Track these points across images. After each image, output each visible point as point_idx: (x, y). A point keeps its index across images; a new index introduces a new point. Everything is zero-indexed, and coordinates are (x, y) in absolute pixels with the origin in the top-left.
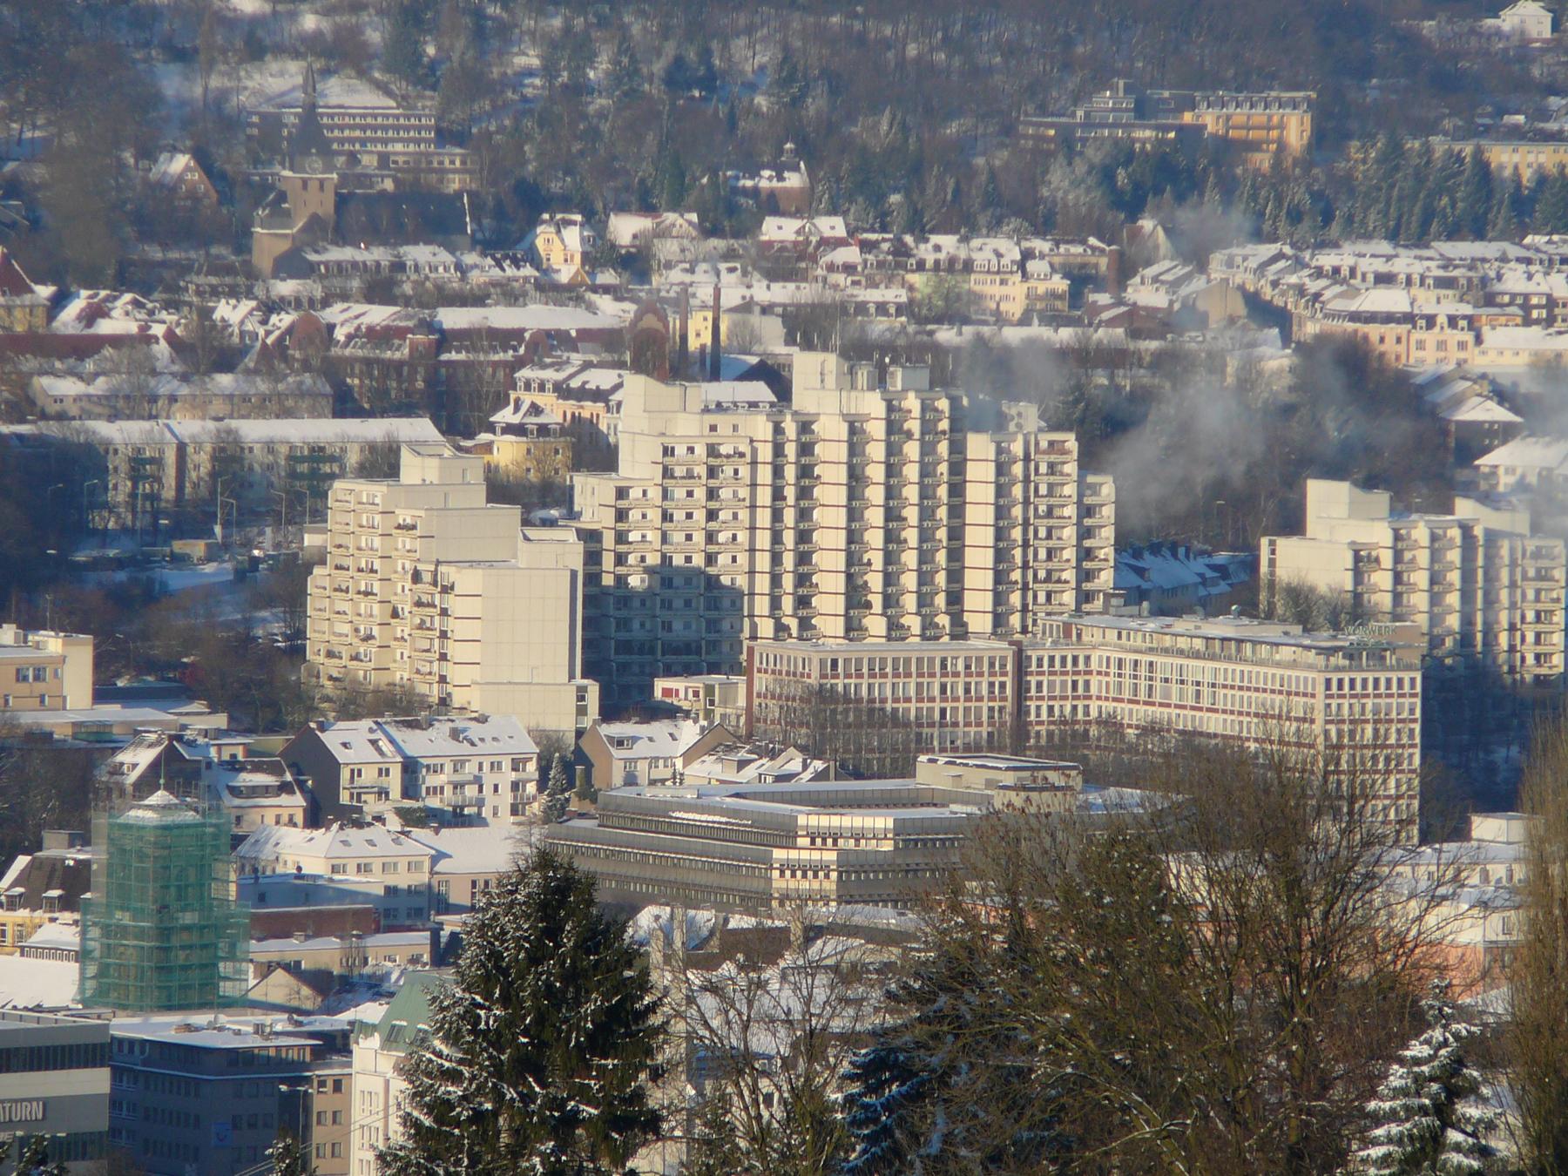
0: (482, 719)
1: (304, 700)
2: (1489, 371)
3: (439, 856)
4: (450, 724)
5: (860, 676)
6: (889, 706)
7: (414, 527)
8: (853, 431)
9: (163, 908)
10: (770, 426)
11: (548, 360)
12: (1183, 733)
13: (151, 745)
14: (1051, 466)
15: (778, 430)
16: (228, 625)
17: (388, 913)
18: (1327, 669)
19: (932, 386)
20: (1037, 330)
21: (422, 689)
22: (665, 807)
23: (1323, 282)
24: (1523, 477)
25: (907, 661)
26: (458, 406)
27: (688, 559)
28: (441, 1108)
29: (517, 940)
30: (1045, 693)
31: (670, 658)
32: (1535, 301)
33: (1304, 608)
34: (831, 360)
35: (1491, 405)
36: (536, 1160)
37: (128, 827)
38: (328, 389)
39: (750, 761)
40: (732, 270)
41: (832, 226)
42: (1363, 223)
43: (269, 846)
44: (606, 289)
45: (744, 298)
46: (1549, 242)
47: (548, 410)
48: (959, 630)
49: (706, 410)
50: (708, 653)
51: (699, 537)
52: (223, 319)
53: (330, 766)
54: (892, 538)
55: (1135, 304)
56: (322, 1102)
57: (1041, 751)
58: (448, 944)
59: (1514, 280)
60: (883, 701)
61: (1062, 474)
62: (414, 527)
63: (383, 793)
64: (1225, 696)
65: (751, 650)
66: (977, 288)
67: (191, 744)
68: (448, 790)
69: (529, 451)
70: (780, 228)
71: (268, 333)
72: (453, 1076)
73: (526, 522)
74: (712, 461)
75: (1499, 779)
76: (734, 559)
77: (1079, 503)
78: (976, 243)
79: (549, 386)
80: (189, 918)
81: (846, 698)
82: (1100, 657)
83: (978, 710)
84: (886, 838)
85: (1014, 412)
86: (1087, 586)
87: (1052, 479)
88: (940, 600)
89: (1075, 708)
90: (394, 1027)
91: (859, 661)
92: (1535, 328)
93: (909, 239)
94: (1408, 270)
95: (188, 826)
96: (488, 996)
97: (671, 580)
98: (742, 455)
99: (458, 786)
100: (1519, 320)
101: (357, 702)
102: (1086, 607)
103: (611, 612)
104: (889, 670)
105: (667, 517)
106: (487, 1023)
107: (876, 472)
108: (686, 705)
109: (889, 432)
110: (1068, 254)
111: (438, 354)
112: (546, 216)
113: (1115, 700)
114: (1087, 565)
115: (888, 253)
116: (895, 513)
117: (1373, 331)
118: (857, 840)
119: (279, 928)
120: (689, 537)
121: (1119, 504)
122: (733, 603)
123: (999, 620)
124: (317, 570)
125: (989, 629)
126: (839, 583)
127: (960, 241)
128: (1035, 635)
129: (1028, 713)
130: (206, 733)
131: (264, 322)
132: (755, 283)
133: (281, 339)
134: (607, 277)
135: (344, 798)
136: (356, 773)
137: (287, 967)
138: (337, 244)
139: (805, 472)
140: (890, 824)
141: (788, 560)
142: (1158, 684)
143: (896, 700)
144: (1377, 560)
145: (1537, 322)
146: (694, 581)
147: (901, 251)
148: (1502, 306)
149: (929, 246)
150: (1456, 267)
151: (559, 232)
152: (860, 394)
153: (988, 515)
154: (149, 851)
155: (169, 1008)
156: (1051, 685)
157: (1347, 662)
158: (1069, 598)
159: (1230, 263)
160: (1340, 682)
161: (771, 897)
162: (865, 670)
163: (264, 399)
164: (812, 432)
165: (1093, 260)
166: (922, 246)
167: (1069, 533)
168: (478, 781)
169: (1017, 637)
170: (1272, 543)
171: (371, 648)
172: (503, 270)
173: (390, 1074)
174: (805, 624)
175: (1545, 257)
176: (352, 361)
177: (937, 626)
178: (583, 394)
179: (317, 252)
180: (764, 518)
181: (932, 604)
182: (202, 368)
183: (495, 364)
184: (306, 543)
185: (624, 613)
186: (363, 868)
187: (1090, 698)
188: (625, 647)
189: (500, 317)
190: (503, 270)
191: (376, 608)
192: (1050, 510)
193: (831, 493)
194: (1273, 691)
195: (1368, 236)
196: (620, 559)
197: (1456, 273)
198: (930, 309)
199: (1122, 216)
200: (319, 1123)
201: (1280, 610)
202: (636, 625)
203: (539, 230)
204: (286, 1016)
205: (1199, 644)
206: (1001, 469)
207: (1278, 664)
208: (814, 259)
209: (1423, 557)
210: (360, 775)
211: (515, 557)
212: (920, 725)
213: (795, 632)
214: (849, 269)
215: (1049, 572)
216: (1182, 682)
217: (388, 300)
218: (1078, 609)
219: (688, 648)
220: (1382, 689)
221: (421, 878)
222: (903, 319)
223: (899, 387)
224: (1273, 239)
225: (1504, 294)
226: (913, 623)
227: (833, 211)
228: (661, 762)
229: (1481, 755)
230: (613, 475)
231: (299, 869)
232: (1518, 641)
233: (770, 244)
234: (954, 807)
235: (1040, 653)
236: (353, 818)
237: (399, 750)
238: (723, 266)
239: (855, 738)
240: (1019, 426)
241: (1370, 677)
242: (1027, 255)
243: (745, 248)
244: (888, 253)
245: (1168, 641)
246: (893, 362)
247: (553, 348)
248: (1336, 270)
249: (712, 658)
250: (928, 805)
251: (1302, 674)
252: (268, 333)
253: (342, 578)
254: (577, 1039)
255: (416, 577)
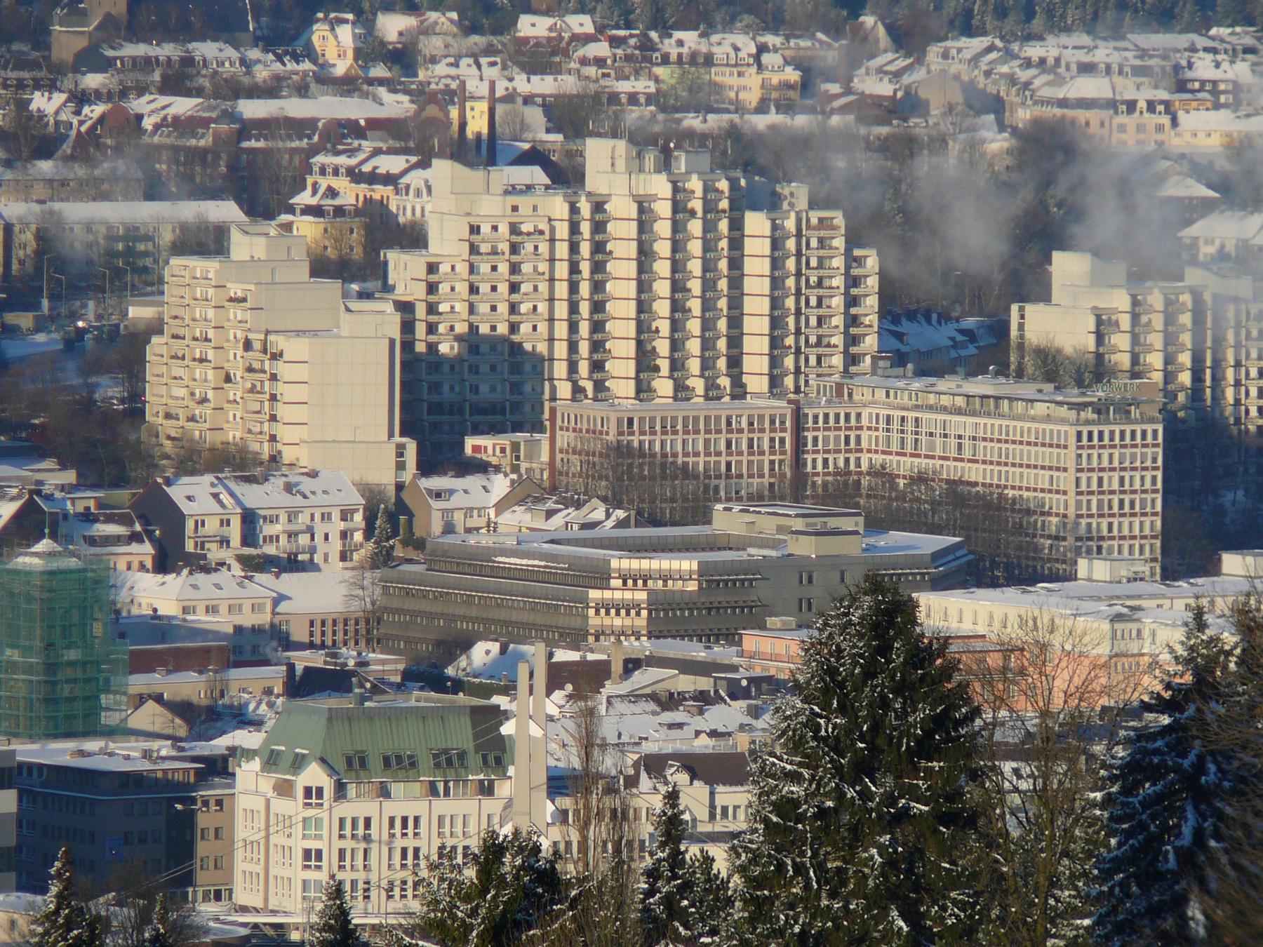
0: (313, 474)
1: (148, 460)
2: (1186, 151)
3: (279, 599)
4: (284, 479)
5: (653, 433)
6: (680, 460)
7: (244, 300)
8: (641, 210)
9: (50, 645)
10: (566, 207)
11: (340, 147)
12: (948, 481)
13: (13, 499)
14: (821, 241)
15: (574, 210)
16: (73, 389)
17: (238, 650)
18: (1078, 422)
19: (712, 171)
20: (774, 117)
21: (254, 447)
22: (487, 554)
23: (1032, 72)
24: (1222, 246)
25: (696, 419)
26: (260, 187)
27: (493, 328)
28: (787, 807)
29: (852, 656)
30: (820, 446)
31: (477, 418)
32: (1222, 87)
33: (1051, 367)
34: (621, 145)
35: (1191, 182)
36: (874, 851)
37: (16, 572)
38: (140, 175)
39: (560, 510)
40: (493, 64)
41: (582, 23)
42: (1063, 17)
43: (125, 590)
44: (381, 82)
45: (507, 89)
46: (1232, 34)
47: (342, 191)
48: (738, 391)
49: (506, 192)
50: (512, 413)
51: (503, 308)
52: (39, 110)
53: (174, 518)
54: (677, 307)
55: (863, 93)
56: (204, 820)
57: (816, 499)
58: (302, 677)
59: (1204, 68)
60: (675, 455)
61: (831, 248)
62: (244, 300)
63: (224, 542)
64: (985, 447)
65: (553, 411)
66: (718, 79)
67: (49, 498)
68: (283, 540)
69: (326, 230)
70: (533, 25)
71: (81, 123)
72: (795, 777)
73: (345, 295)
74: (515, 238)
75: (1227, 520)
76: (535, 328)
77: (847, 274)
78: (715, 38)
79: (342, 170)
80: (72, 655)
81: (641, 453)
82: (870, 414)
83: (761, 463)
84: (691, 579)
85: (786, 192)
86: (853, 350)
87: (822, 253)
88: (722, 364)
89: (847, 460)
90: (273, 751)
91: (653, 420)
92: (1222, 111)
93: (654, 35)
94: (1109, 60)
95: (71, 571)
96: (826, 706)
97: (477, 347)
98: (542, 233)
99: (292, 535)
100: (1209, 104)
101: (194, 459)
102: (853, 369)
103: (424, 376)
104: (679, 427)
105: (473, 290)
106: (826, 731)
107: (663, 248)
108: (494, 461)
109: (675, 211)
110: (798, 48)
111: (239, 140)
112: (320, 15)
113: (884, 452)
114: (853, 331)
115: (635, 48)
116: (681, 285)
117: (1082, 115)
118: (665, 581)
119: (142, 663)
120: (494, 308)
121: (883, 276)
122: (534, 367)
123: (775, 381)
124: (155, 340)
125: (765, 388)
126: (630, 349)
127: (701, 36)
128: (806, 394)
129: (805, 465)
130: (62, 488)
131: (78, 113)
132: (516, 77)
133: (93, 128)
134: (379, 71)
135: (190, 546)
136: (199, 524)
137: (159, 699)
138: (131, 41)
139: (598, 247)
140: (695, 566)
141: (584, 328)
142: (923, 438)
143: (686, 455)
144: (1117, 324)
145: (1226, 106)
146: (499, 348)
147: (647, 46)
148: (1193, 91)
149: (673, 41)
150: (1151, 57)
151: (333, 29)
152: (648, 177)
153: (765, 286)
154: (36, 594)
155: (68, 735)
156: (826, 439)
157: (1095, 416)
158: (837, 360)
159: (945, 56)
160: (1090, 434)
161: (587, 633)
162: (658, 428)
163: (81, 183)
164: (605, 211)
165: (822, 53)
166: (666, 41)
167: (837, 302)
168: (310, 531)
169: (792, 396)
170: (1021, 309)
171: (207, 410)
172: (284, 65)
173: (270, 794)
174: (599, 386)
175: (1229, 47)
176: (159, 148)
177: (718, 387)
178: (373, 178)
179: (113, 48)
180: (562, 290)
181: (714, 367)
182: (24, 155)
183: (294, 151)
184: (130, 315)
185: (434, 378)
186: (209, 610)
187: (861, 451)
188: (436, 408)
189: (295, 108)
190: (284, 65)
191: (210, 374)
192: (820, 280)
193: (622, 269)
194: (1014, 442)
195: (1067, 30)
196: (432, 329)
197: (1153, 62)
198: (676, 99)
199: (845, 13)
200: (203, 838)
201: (1030, 370)
202: (446, 388)
203: (315, 27)
204: (169, 742)
205: (960, 401)
206: (776, 244)
207: (1033, 419)
208: (566, 54)
209: (1158, 322)
210: (203, 525)
211: (338, 327)
212: (709, 477)
213: (590, 393)
214: (600, 62)
215: (820, 338)
216: (945, 436)
217: (188, 93)
218: (846, 371)
219: (494, 409)
220: (1128, 440)
221: (264, 619)
222: (652, 108)
223: (683, 169)
224: (984, 33)
225: (1194, 81)
226: (698, 384)
227: (581, 10)
228: (475, 512)
229: (1211, 499)
230: (424, 252)
231: (155, 610)
232: (1243, 396)
233: (526, 40)
234: (751, 551)
235: (816, 411)
236: (199, 564)
237: (238, 502)
238: (484, 61)
239: (653, 491)
240: (792, 205)
241: (1117, 429)
242: (762, 49)
243: (504, 45)
244: (635, 48)
245: (932, 399)
246: (677, 147)
247: (344, 136)
248: (1043, 61)
249: (515, 418)
250: (725, 549)
251: (1056, 428)
252: (81, 123)
253: (178, 346)
254: (908, 744)
255: (248, 345)
